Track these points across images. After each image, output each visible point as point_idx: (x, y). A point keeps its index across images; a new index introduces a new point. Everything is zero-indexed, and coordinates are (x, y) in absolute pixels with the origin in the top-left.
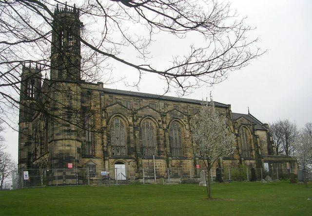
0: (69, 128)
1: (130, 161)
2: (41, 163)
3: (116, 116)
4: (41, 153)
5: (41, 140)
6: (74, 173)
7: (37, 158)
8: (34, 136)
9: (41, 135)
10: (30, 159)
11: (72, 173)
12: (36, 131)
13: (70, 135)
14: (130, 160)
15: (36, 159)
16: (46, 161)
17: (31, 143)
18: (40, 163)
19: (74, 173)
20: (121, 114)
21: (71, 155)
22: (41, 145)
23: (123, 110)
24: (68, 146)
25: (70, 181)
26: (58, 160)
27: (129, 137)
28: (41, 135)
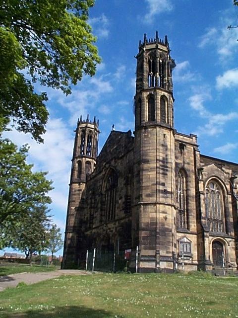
0: (165, 189)
1: (230, 241)
2: (100, 234)
3: (212, 179)
4: (101, 221)
5: (102, 205)
6: (170, 252)
7: (94, 226)
8: (89, 201)
9: (102, 198)
10: (81, 227)
11: (167, 252)
12: (93, 193)
13: (167, 197)
14: (230, 239)
15: (91, 228)
16: (112, 231)
17: (84, 208)
18: (99, 234)
19: (170, 252)
20: (220, 179)
21: (166, 227)
22: (102, 210)
23: (220, 173)
24: (164, 212)
25: (163, 265)
26: (148, 232)
27: (226, 209)
28: (102, 198)
